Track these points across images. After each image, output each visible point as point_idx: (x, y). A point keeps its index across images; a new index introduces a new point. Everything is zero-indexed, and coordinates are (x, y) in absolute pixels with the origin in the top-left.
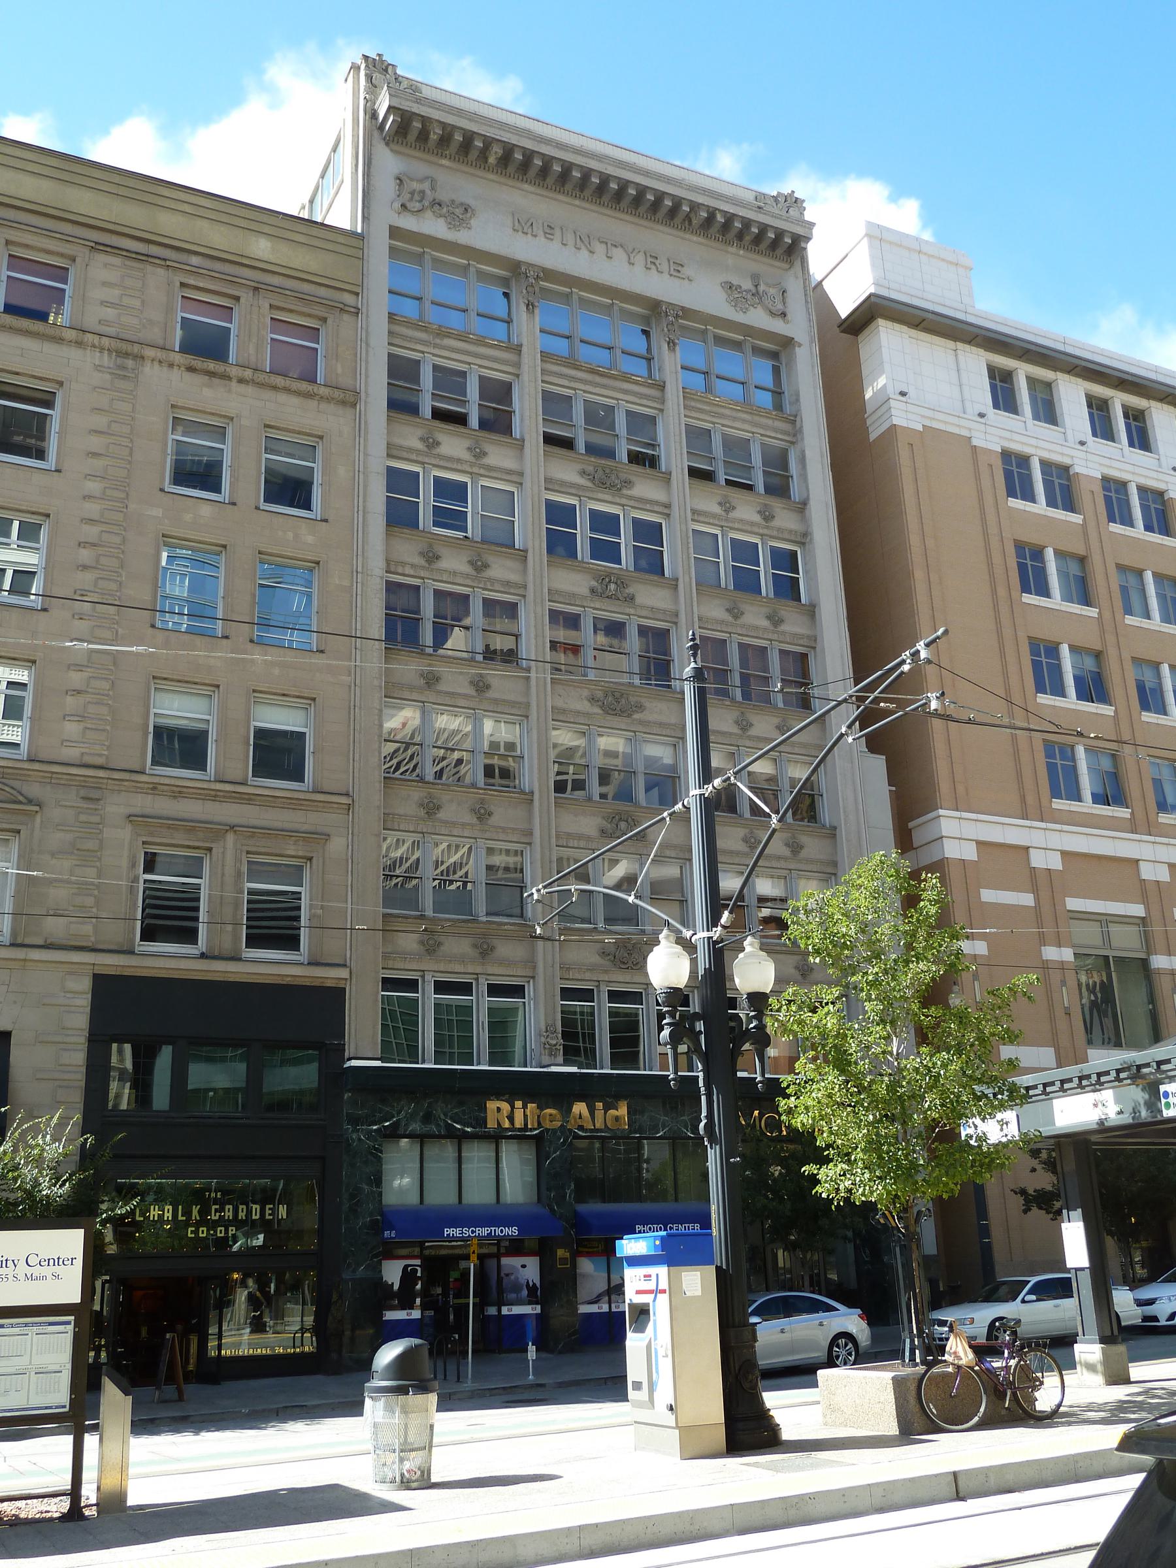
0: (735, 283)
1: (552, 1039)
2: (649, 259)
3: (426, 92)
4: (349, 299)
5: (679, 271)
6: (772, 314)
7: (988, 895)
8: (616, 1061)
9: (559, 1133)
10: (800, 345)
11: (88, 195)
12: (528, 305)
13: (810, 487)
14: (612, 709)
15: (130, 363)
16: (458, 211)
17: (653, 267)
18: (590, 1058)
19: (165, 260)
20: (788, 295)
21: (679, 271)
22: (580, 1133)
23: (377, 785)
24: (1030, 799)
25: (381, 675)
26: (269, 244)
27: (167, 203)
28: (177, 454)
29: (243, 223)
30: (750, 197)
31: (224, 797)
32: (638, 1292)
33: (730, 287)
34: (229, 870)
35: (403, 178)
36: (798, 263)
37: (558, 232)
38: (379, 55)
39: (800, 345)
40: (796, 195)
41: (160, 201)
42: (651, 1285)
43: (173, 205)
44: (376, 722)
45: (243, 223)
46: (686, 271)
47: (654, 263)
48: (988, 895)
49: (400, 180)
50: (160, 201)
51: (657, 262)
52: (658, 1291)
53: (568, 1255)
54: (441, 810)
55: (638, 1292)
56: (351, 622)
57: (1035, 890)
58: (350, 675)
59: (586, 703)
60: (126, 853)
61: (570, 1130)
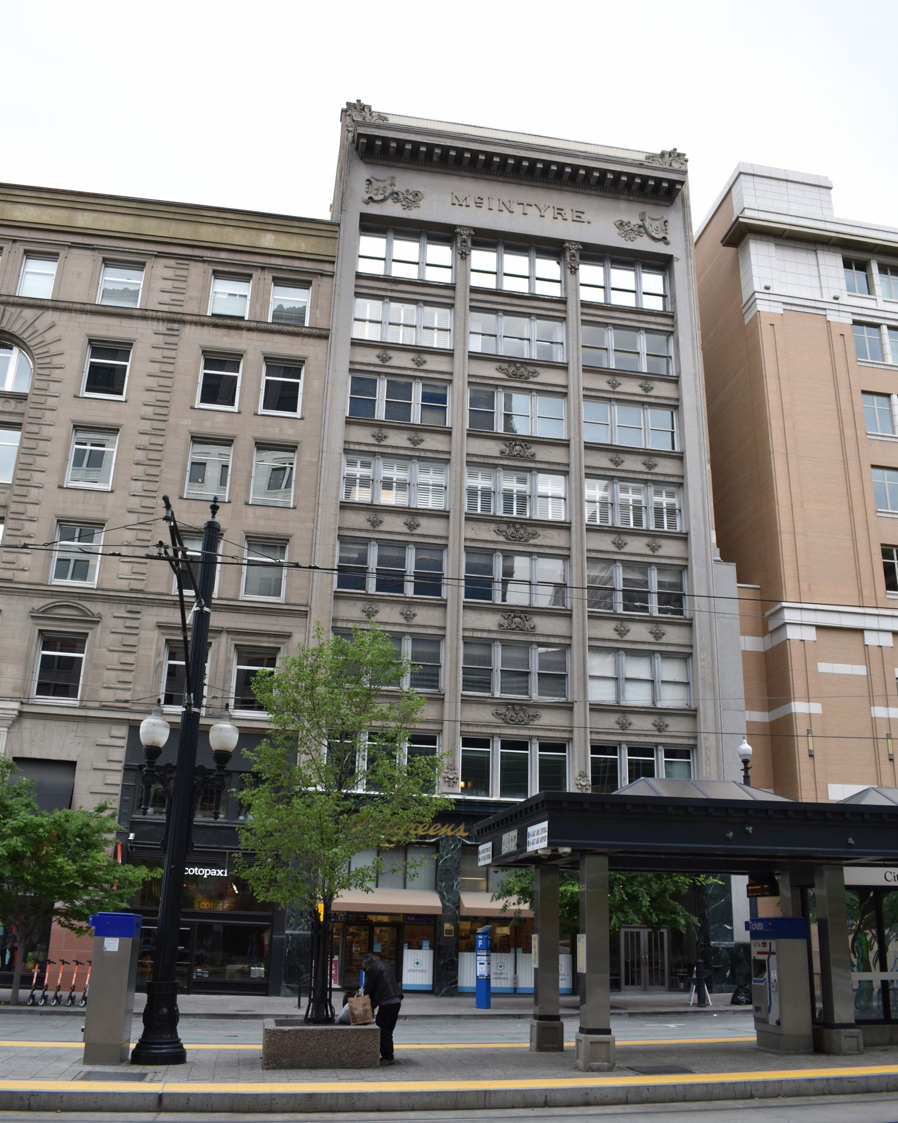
0: (626, 220)
1: (451, 774)
2: (557, 211)
3: (392, 120)
4: (328, 268)
5: (580, 217)
6: (654, 239)
7: (824, 667)
8: (505, 790)
9: (451, 842)
10: (678, 260)
11: (154, 222)
12: (461, 254)
13: (681, 364)
14: (513, 537)
15: (176, 326)
16: (410, 197)
17: (559, 216)
18: (485, 788)
19: (202, 257)
20: (669, 225)
21: (580, 217)
22: (468, 842)
23: (329, 597)
24: (867, 592)
25: (336, 522)
26: (273, 237)
27: (205, 220)
28: (564, 684)
29: (256, 226)
30: (641, 157)
31: (221, 608)
32: (759, 953)
33: (621, 225)
34: (222, 657)
35: (372, 180)
36: (678, 200)
37: (485, 202)
38: (358, 101)
39: (678, 260)
40: (678, 151)
41: (201, 220)
42: (767, 949)
43: (210, 221)
44: (331, 554)
45: (256, 226)
46: (584, 217)
47: (560, 214)
48: (824, 667)
49: (369, 182)
50: (201, 220)
51: (563, 213)
52: (770, 953)
53: (452, 928)
54: (379, 614)
55: (759, 953)
56: (316, 486)
57: (868, 663)
58: (314, 522)
59: (493, 533)
60: (154, 647)
61: (459, 840)
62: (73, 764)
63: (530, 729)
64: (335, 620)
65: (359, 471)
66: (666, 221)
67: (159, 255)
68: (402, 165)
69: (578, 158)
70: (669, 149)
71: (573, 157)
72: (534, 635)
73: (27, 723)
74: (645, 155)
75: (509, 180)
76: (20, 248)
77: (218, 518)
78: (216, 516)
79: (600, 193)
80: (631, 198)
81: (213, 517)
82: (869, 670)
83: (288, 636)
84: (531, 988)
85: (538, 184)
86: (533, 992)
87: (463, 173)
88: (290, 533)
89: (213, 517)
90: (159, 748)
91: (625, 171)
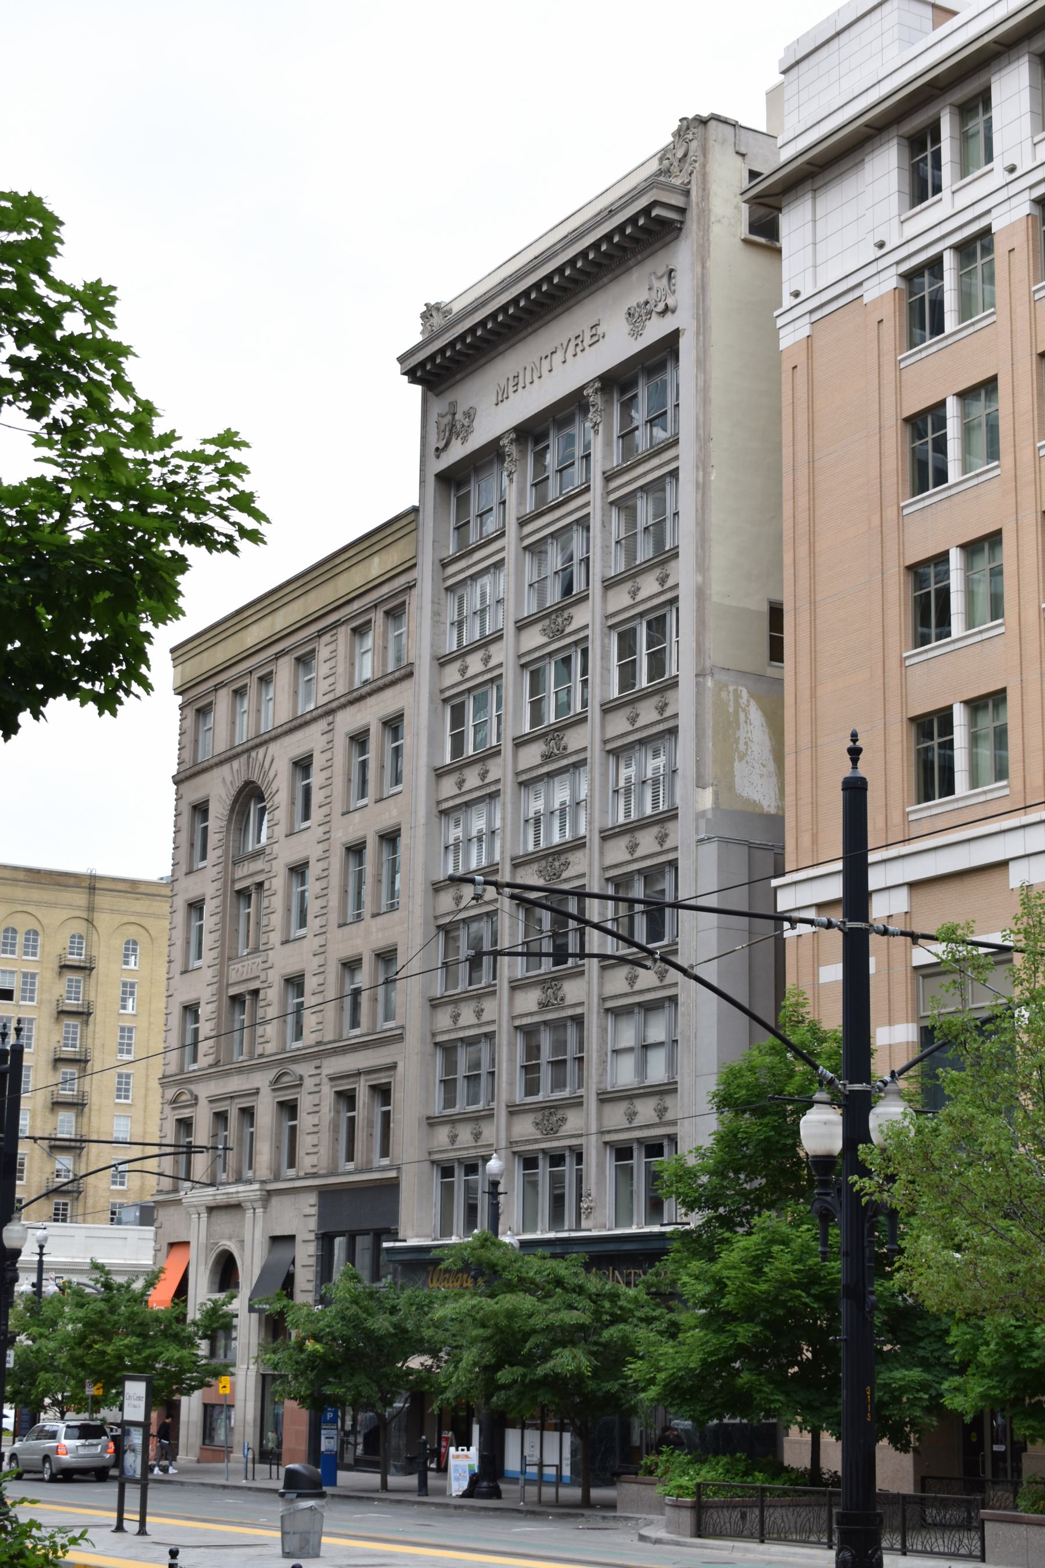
62: (291, 1238)
63: (558, 1139)
64: (434, 1035)
65: (455, 833)
66: (672, 271)
67: (321, 634)
68: (458, 377)
69: (557, 255)
70: (675, 125)
71: (550, 260)
72: (563, 1008)
73: (275, 1200)
74: (656, 161)
75: (536, 326)
76: (344, 632)
77: (862, 771)
78: (860, 764)
79: (610, 276)
80: (639, 257)
81: (855, 766)
82: (815, 975)
83: (393, 1067)
84: (552, 1475)
85: (559, 310)
86: (536, 1478)
87: (501, 348)
88: (390, 942)
89: (855, 766)
90: (834, 1157)
91: (599, 237)
